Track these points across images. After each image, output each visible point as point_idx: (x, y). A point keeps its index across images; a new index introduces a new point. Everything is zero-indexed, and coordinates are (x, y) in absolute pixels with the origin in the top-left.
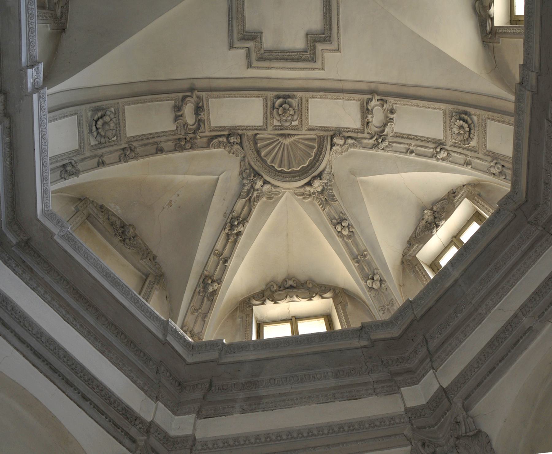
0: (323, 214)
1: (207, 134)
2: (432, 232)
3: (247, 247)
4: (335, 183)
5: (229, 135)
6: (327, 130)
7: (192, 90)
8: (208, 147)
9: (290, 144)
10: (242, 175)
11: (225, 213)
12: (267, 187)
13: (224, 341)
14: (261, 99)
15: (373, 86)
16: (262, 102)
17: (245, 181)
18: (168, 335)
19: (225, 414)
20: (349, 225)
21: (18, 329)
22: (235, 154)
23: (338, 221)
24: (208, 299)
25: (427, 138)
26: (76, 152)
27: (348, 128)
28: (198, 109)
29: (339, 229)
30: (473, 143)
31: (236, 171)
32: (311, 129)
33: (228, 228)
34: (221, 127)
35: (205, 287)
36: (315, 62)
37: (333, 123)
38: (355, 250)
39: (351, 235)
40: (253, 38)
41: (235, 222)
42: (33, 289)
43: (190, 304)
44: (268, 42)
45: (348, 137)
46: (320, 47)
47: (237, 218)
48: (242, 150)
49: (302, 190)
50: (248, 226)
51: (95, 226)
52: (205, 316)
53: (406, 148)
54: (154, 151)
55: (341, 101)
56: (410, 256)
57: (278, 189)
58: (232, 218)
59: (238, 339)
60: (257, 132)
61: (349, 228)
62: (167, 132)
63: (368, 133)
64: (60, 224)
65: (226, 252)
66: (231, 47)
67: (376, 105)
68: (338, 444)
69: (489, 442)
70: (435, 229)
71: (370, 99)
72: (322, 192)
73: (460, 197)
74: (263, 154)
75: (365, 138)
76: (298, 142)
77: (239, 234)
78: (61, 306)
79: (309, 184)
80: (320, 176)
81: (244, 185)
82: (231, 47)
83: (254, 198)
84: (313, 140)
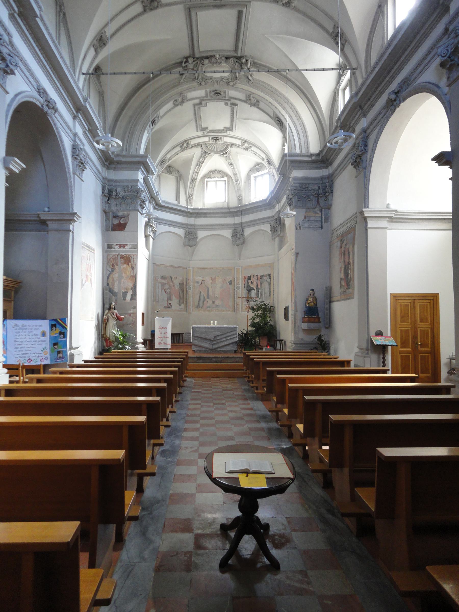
1: (191, 146)
7: (186, 141)
35: (193, 181)
65: (198, 171)
77: (201, 166)
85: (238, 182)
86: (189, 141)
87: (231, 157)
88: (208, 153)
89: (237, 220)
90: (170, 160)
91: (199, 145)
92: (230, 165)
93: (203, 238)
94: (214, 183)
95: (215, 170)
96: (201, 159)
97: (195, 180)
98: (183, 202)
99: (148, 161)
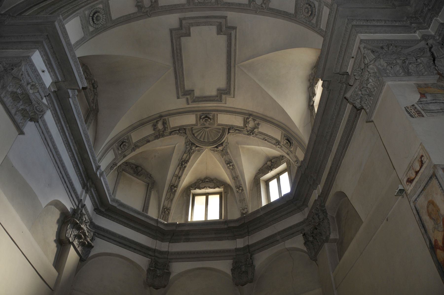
0: (223, 159)
1: (169, 131)
2: (269, 171)
3: (188, 170)
4: (229, 146)
5: (180, 129)
6: (227, 126)
7: (161, 117)
8: (170, 135)
9: (209, 130)
10: (186, 144)
11: (179, 159)
12: (197, 148)
13: (178, 223)
14: (195, 115)
15: (250, 113)
16: (195, 116)
17: (187, 147)
18: (159, 224)
19: (179, 242)
20: (233, 165)
21: (113, 238)
22: (183, 136)
23: (229, 162)
24: (173, 194)
25: (273, 137)
26: (115, 159)
27: (237, 126)
28: (164, 123)
29: (228, 166)
30: (292, 149)
31: (184, 142)
32: (219, 125)
33: (180, 165)
34: (176, 127)
35: (171, 189)
36: (221, 102)
37: (230, 123)
38: (234, 175)
39: (234, 169)
40: (189, 94)
41: (183, 163)
42: (113, 221)
43: (166, 197)
44: (197, 93)
45: (236, 130)
46: (224, 96)
47: (184, 161)
48: (186, 135)
49: (213, 149)
50: (189, 164)
51: (126, 172)
52: (172, 200)
53: (263, 138)
54: (146, 142)
55: (234, 116)
56: (258, 177)
57: (202, 148)
58: (182, 161)
59: (183, 222)
60: (192, 127)
61: (232, 166)
62: (151, 134)
63: (246, 129)
64: (117, 202)
65: (179, 175)
66: (178, 98)
67: (251, 120)
68: (212, 257)
69: (254, 267)
70: (270, 171)
71: (248, 118)
72: (222, 150)
73: (284, 161)
74: (195, 136)
75: (245, 131)
76: (213, 130)
77: (185, 167)
78: (122, 223)
79: (217, 147)
80: (222, 144)
81: (187, 148)
82: (178, 98)
83: (192, 153)
84: (220, 129)
85: (241, 188)
86: (166, 117)
87: (228, 151)
88: (195, 144)
89: (240, 243)
90: (136, 146)
91: (181, 130)
92: (227, 164)
93: (181, 275)
94: (204, 197)
95: (206, 178)
96: (185, 155)
97: (175, 187)
98: (153, 213)
99: (56, 24)
